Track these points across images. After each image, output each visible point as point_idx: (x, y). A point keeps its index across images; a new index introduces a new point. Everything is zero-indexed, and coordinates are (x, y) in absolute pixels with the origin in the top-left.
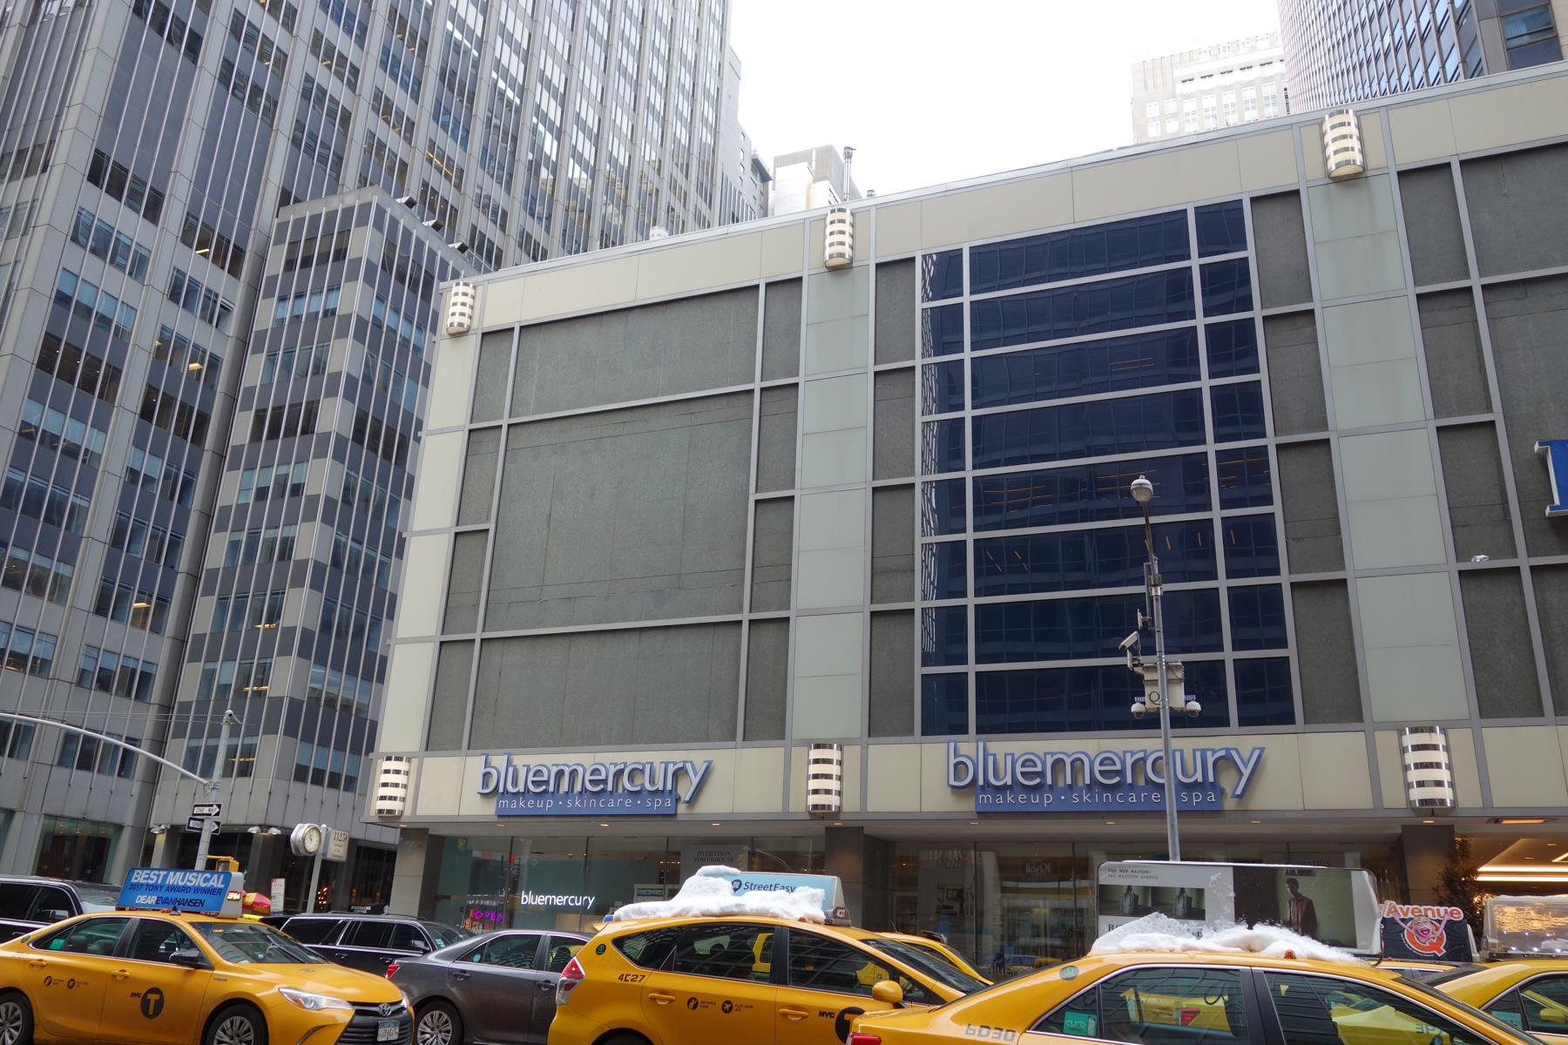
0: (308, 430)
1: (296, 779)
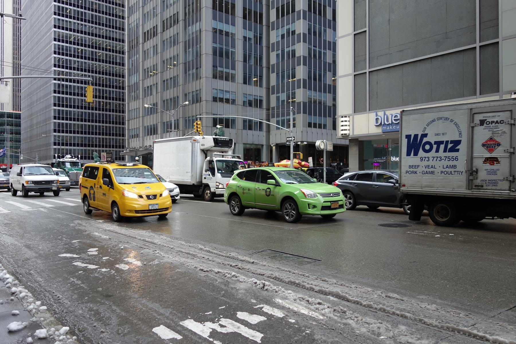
0: (293, 11)
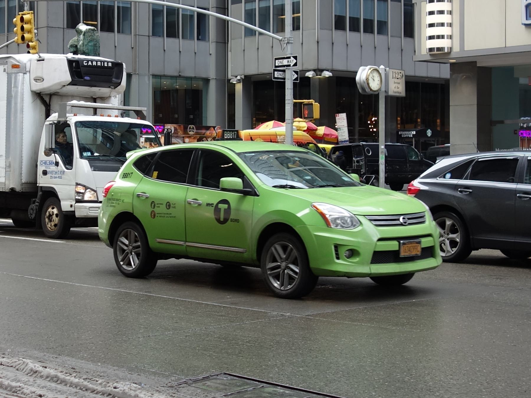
1: (337, 28)
